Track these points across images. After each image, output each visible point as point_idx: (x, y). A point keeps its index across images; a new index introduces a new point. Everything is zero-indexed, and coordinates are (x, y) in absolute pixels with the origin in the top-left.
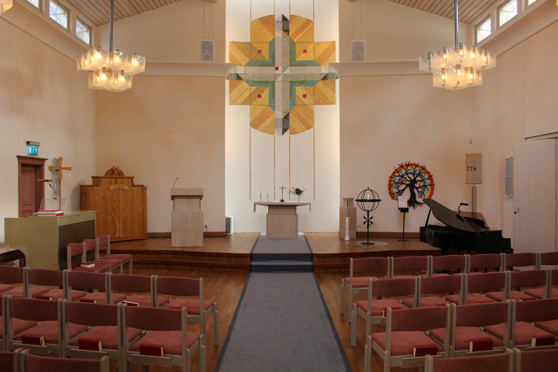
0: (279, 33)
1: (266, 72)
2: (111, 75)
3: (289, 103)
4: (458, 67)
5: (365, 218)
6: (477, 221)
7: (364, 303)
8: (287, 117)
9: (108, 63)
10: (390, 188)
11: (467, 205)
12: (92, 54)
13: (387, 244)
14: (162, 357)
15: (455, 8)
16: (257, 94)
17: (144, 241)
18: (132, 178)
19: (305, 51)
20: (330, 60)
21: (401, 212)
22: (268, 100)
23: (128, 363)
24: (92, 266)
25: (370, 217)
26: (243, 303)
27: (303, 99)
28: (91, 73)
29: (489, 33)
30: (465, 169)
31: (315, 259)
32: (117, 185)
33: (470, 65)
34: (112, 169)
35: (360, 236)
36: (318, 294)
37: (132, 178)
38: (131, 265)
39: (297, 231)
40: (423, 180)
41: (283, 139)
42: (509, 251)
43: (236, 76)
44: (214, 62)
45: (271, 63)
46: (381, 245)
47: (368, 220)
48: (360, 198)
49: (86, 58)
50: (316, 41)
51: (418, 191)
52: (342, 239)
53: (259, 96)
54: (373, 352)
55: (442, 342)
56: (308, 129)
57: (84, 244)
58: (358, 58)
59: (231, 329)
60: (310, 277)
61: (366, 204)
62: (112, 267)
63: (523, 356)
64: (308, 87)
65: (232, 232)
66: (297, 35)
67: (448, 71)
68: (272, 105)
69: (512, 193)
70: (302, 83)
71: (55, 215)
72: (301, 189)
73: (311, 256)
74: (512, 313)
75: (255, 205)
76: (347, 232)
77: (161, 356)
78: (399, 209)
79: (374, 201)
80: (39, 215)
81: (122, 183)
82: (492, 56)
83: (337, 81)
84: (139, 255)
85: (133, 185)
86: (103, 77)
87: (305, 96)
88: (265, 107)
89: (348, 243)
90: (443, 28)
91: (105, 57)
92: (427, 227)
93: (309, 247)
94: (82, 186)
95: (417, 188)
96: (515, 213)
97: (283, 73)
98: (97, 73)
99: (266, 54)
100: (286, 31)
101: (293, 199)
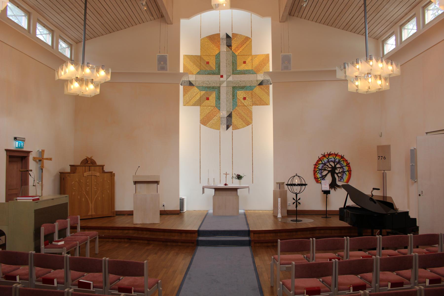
0: (224, 48)
1: (213, 79)
2: (83, 83)
3: (232, 104)
5: (293, 199)
6: (388, 204)
7: (288, 282)
8: (230, 116)
10: (314, 174)
11: (379, 189)
12: (67, 66)
13: (312, 221)
15: (365, 27)
16: (205, 97)
17: (112, 218)
18: (103, 166)
19: (245, 62)
20: (265, 70)
21: (324, 193)
22: (214, 102)
24: (62, 243)
25: (298, 199)
27: (243, 101)
28: (66, 82)
29: (394, 47)
30: (376, 157)
31: (252, 234)
32: (90, 172)
33: (378, 73)
34: (86, 159)
35: (290, 213)
36: (252, 267)
37: (103, 166)
38: (97, 240)
39: (238, 209)
40: (342, 167)
42: (415, 229)
43: (188, 83)
44: (168, 71)
45: (217, 72)
46: (308, 222)
47: (297, 201)
48: (289, 183)
49: (62, 69)
50: (253, 53)
51: (338, 176)
52: (275, 217)
53: (208, 99)
56: (248, 125)
57: (56, 224)
58: (286, 68)
60: (247, 250)
61: (295, 188)
62: (80, 243)
63: (419, 256)
64: (247, 91)
65: (185, 210)
66: (238, 50)
67: (360, 79)
68: (218, 106)
69: (417, 178)
70: (243, 88)
71: (32, 200)
72: (241, 175)
73: (248, 233)
74: (416, 263)
75: (203, 188)
76: (279, 210)
78: (323, 191)
79: (291, 185)
80: (18, 200)
81: (94, 171)
82: (397, 65)
83: (271, 87)
84: (106, 231)
85: (104, 172)
88: (212, 108)
89: (280, 220)
90: (358, 42)
91: (77, 69)
93: (248, 224)
94: (61, 173)
95: (337, 174)
96: (420, 195)
97: (226, 81)
98: (71, 82)
99: (213, 64)
100: (229, 46)
101: (234, 184)
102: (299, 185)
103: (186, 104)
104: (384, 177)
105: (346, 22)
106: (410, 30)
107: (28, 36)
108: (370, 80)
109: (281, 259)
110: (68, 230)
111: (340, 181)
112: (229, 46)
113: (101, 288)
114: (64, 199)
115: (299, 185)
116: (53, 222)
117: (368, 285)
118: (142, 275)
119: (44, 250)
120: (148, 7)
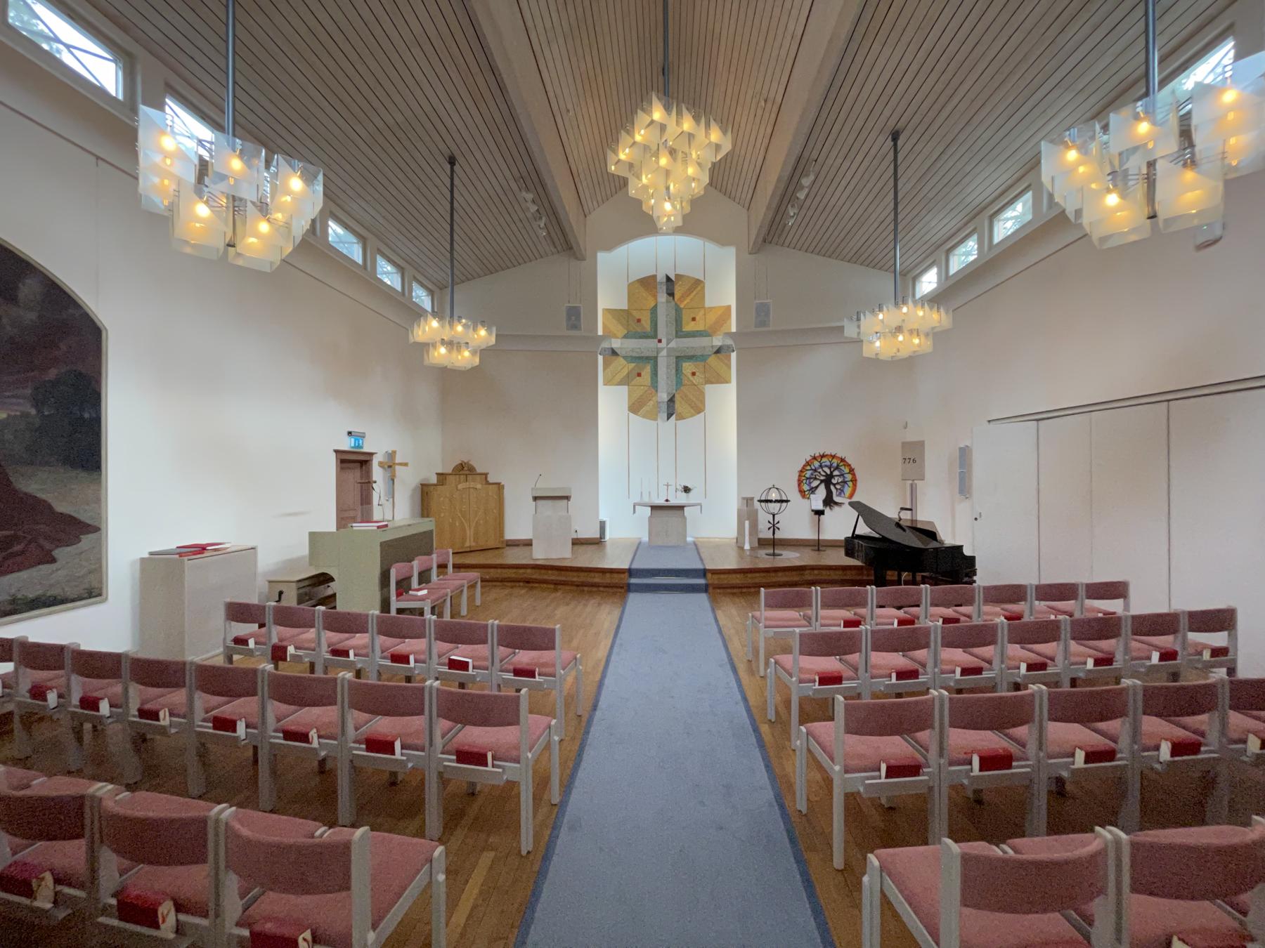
0: (662, 297)
1: (647, 346)
4: (899, 329)
9: (447, 334)
12: (426, 320)
14: (490, 768)
15: (895, 248)
18: (486, 475)
19: (694, 319)
20: (724, 329)
23: (440, 774)
24: (425, 592)
26: (618, 641)
28: (425, 347)
29: (934, 286)
30: (900, 461)
31: (709, 575)
33: (915, 327)
35: (763, 543)
37: (486, 475)
40: (842, 475)
41: (667, 427)
45: (654, 335)
46: (791, 558)
50: (707, 304)
52: (741, 548)
53: (639, 375)
54: (886, 902)
55: (927, 751)
57: (415, 563)
58: (763, 323)
59: (600, 685)
60: (703, 598)
65: (608, 537)
77: (486, 765)
79: (782, 501)
83: (734, 355)
85: (487, 483)
86: (443, 350)
87: (694, 374)
92: (855, 537)
93: (701, 559)
97: (666, 346)
98: (434, 345)
99: (646, 324)
100: (671, 294)
101: (680, 499)
102: (777, 501)
103: (607, 382)
104: (913, 489)
105: (855, 250)
106: (967, 254)
107: (364, 276)
108: (901, 338)
109: (766, 619)
110: (434, 571)
111: (839, 495)
112: (671, 294)
113: (487, 669)
114: (427, 525)
115: (777, 501)
116: (410, 561)
117: (921, 670)
118: (553, 648)
119: (395, 604)
120: (549, 233)
